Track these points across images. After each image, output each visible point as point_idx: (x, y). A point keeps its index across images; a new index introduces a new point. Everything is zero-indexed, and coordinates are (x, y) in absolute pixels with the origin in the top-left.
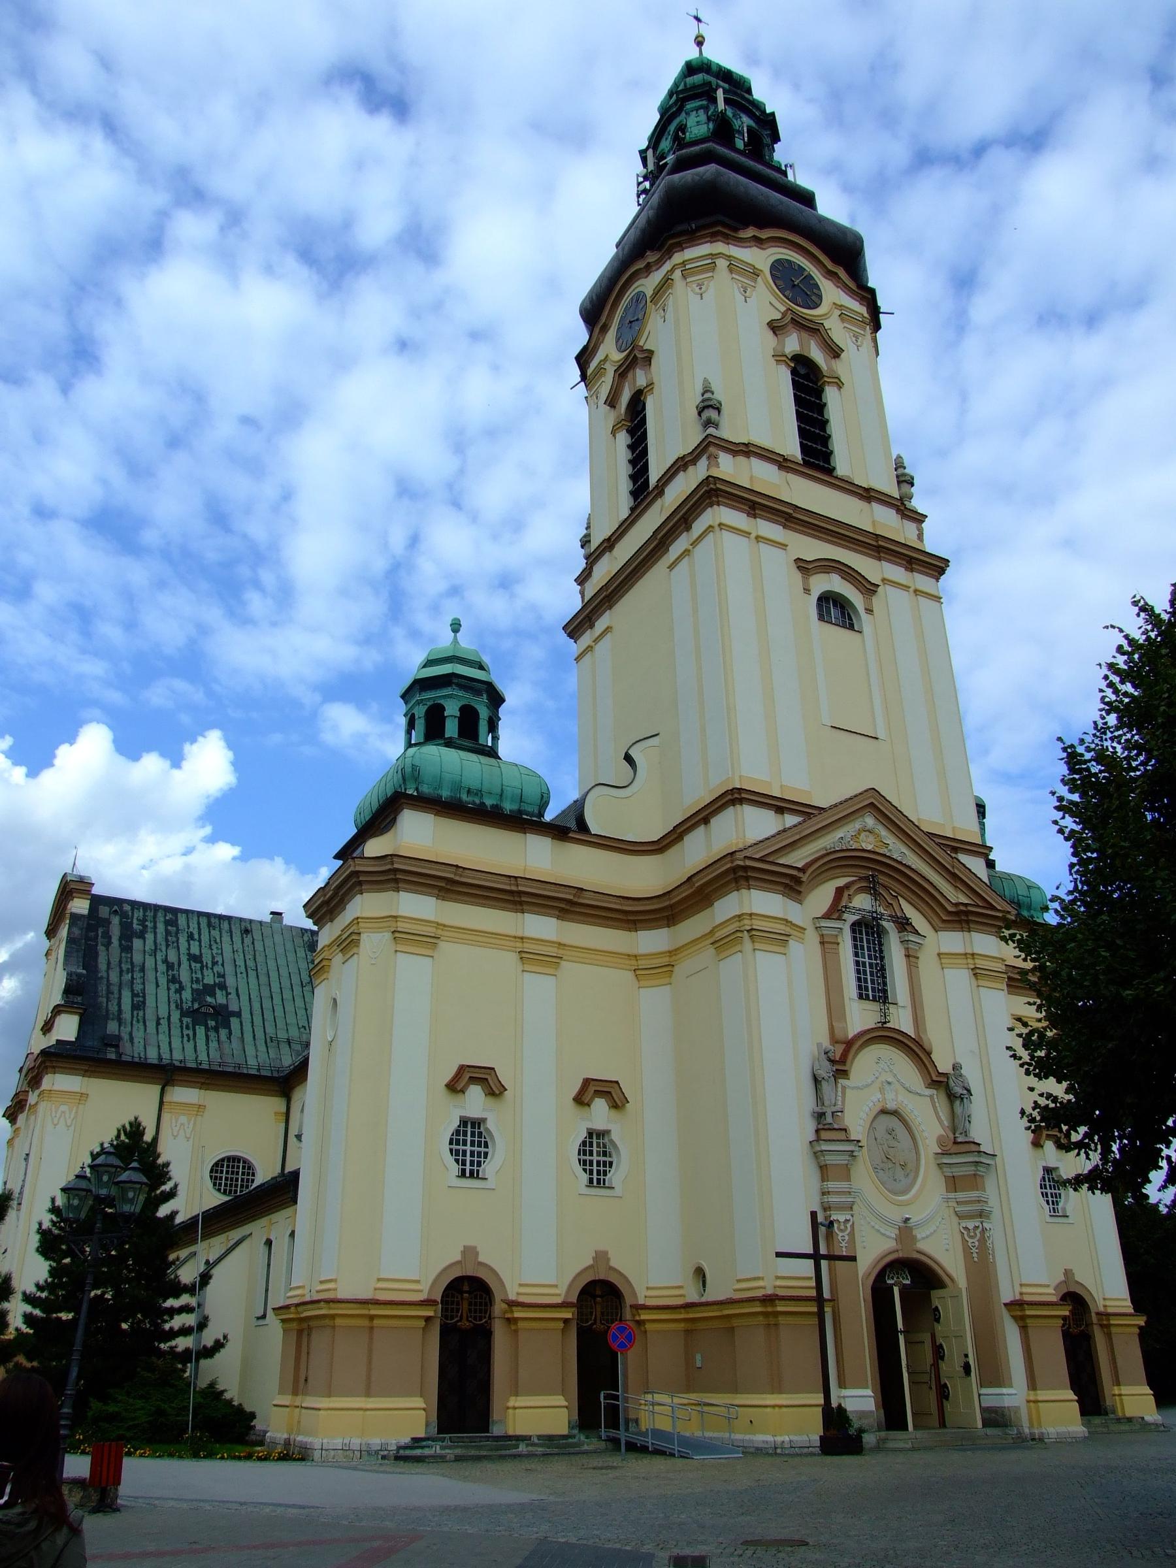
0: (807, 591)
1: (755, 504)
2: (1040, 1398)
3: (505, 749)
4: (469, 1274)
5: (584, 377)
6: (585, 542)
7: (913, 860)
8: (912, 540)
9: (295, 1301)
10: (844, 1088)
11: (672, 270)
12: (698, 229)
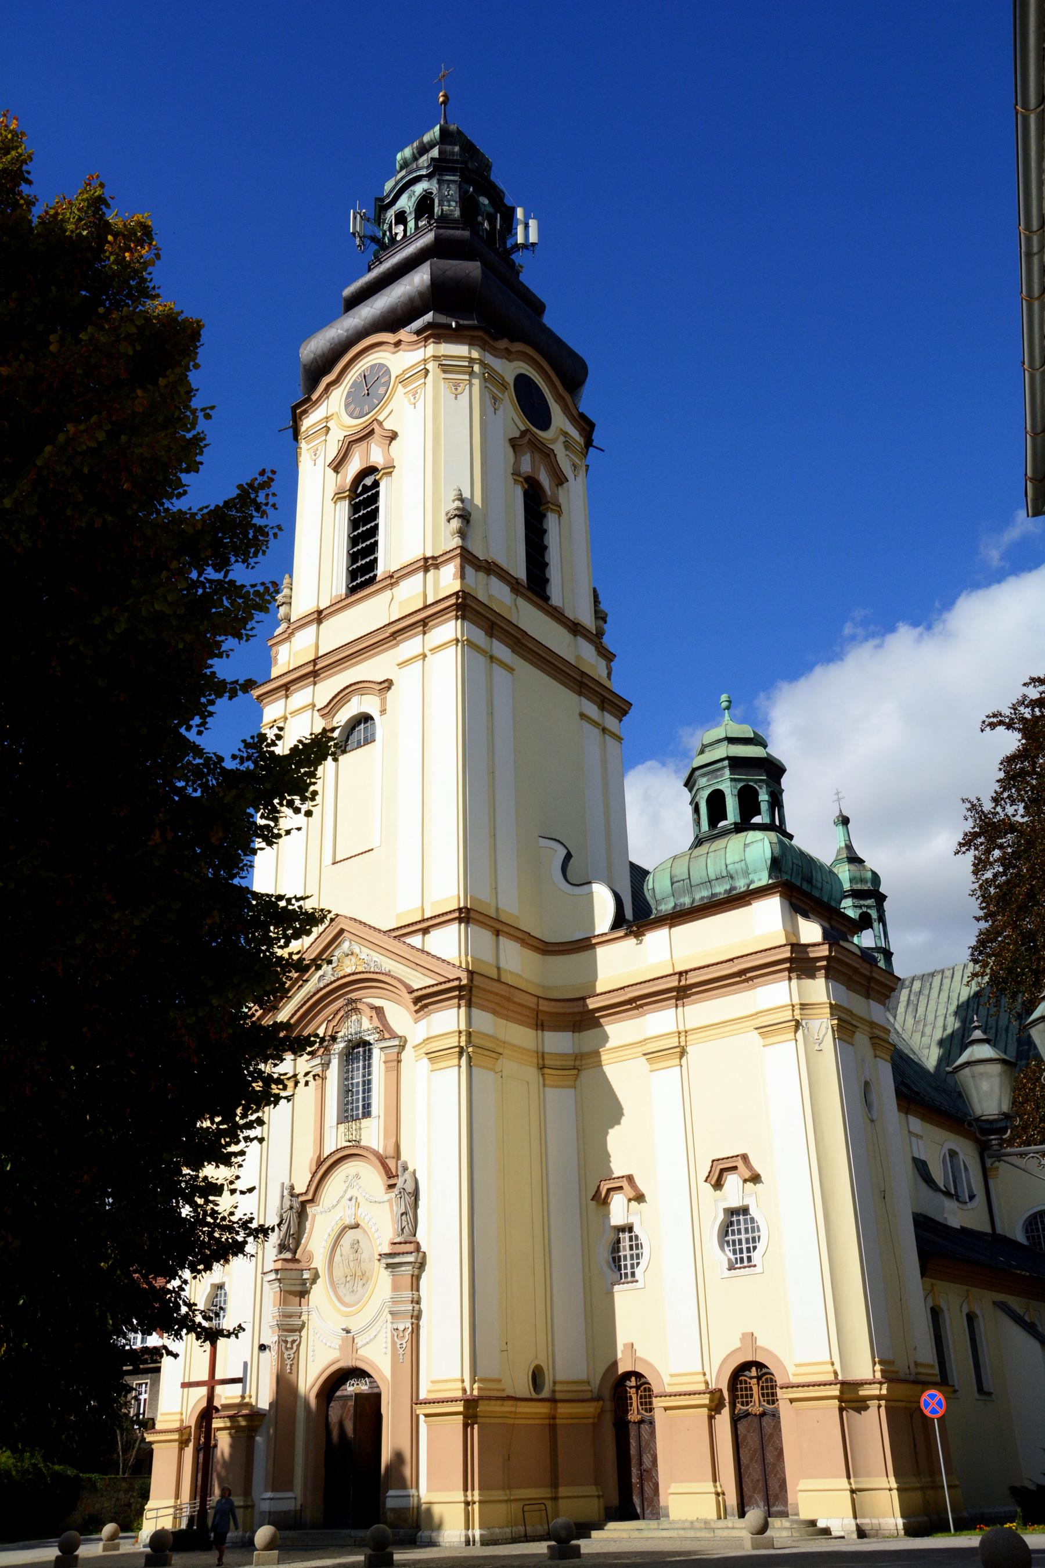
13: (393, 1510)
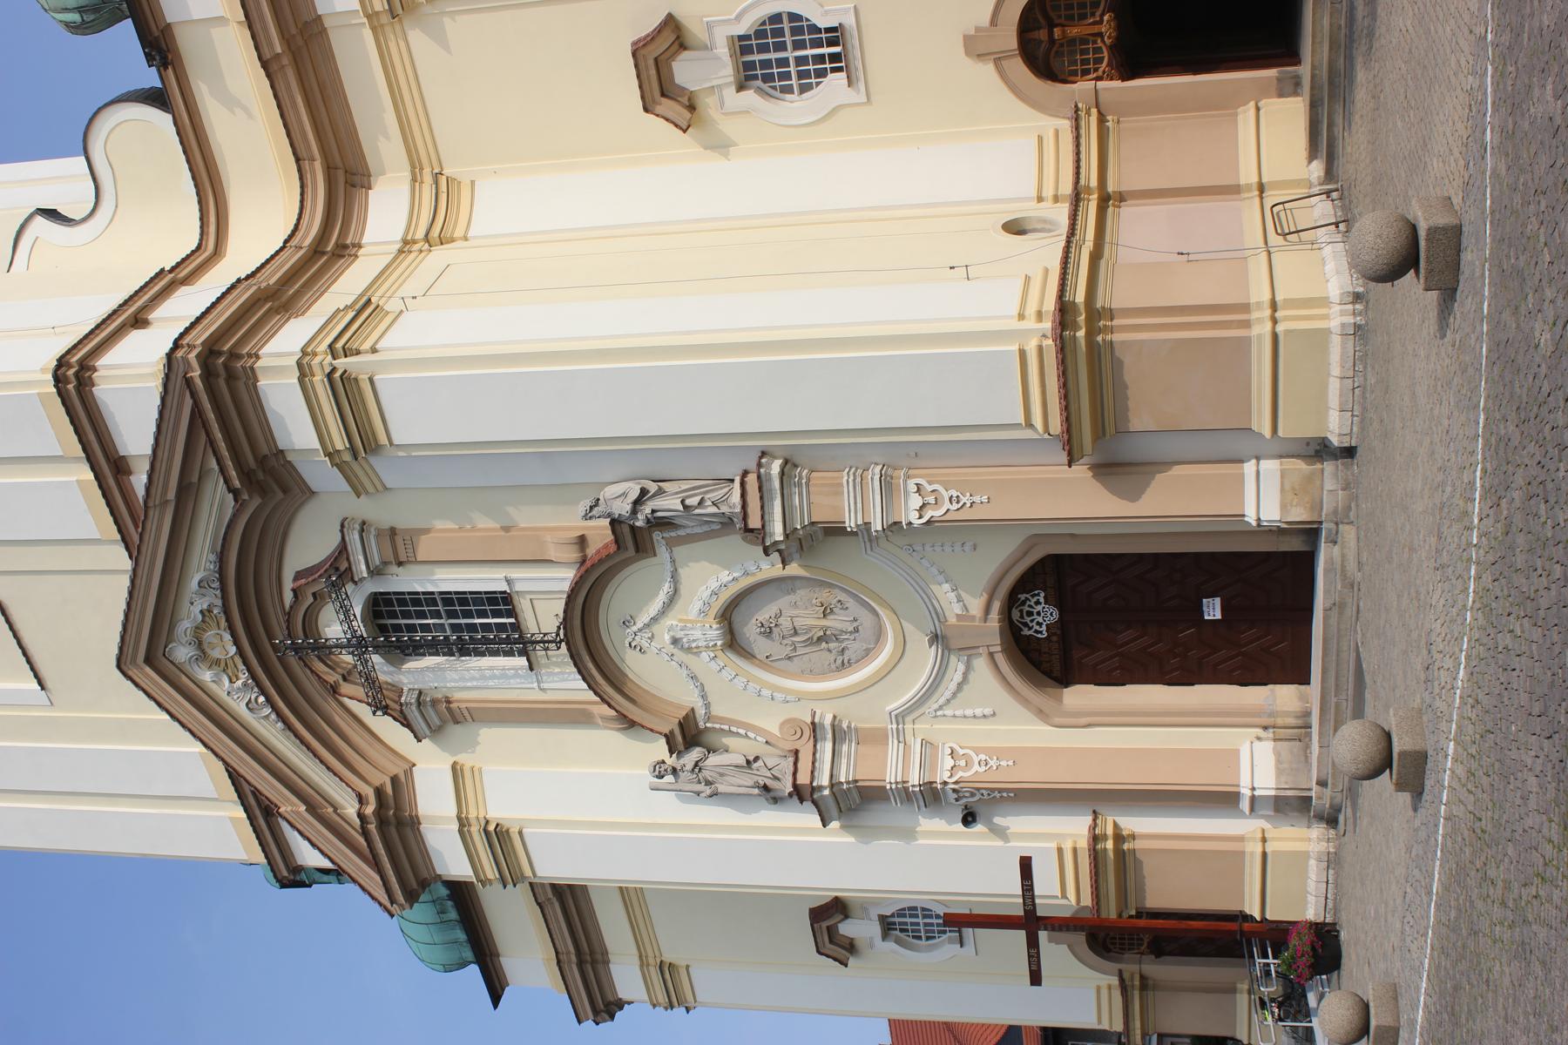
2: (1267, 297)
7: (201, 564)
13: (1284, 507)
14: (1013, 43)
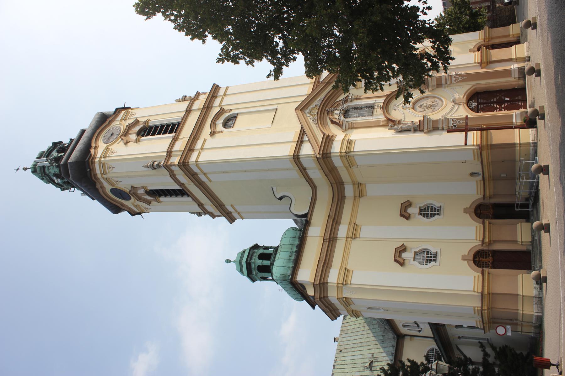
0: (222, 132)
1: (190, 149)
3: (275, 243)
4: (472, 258)
5: (140, 214)
6: (199, 214)
8: (206, 96)
9: (482, 324)
10: (404, 121)
11: (104, 178)
12: (90, 168)
14: (473, 210)
